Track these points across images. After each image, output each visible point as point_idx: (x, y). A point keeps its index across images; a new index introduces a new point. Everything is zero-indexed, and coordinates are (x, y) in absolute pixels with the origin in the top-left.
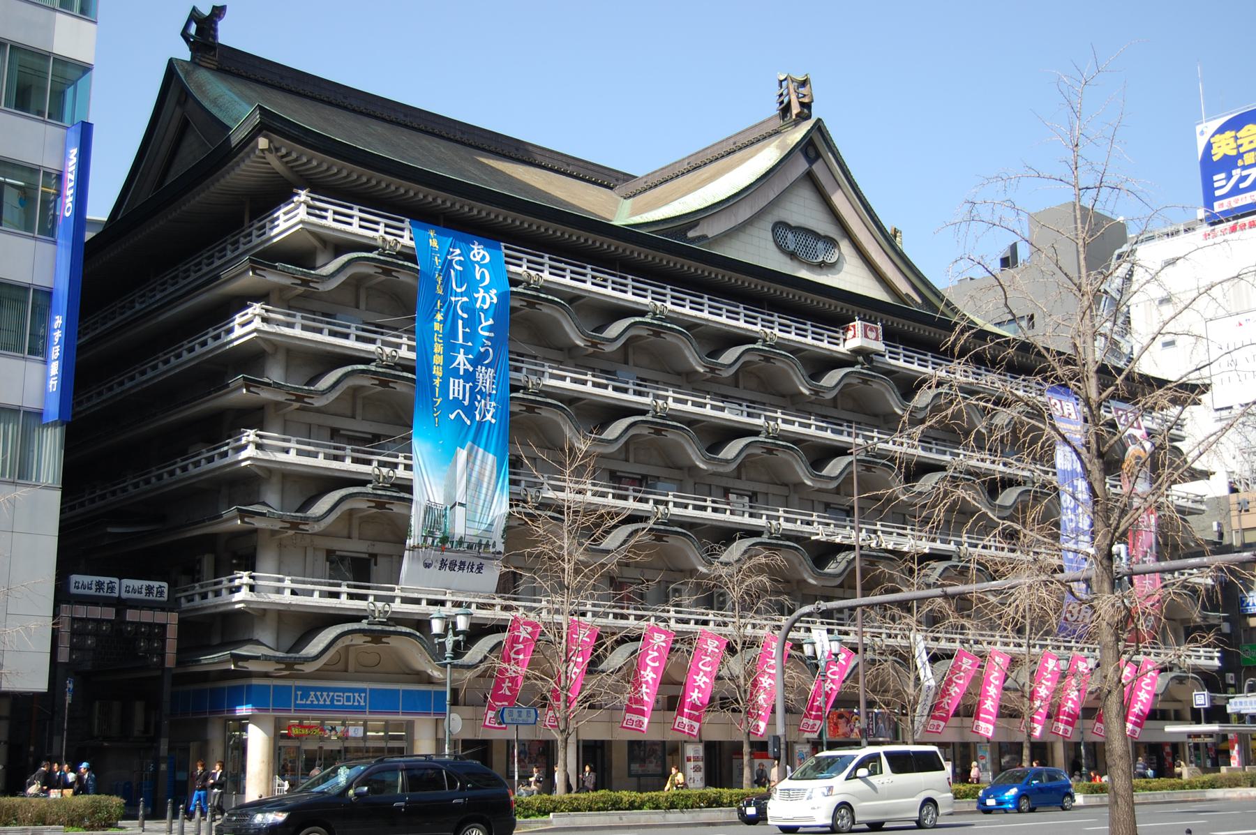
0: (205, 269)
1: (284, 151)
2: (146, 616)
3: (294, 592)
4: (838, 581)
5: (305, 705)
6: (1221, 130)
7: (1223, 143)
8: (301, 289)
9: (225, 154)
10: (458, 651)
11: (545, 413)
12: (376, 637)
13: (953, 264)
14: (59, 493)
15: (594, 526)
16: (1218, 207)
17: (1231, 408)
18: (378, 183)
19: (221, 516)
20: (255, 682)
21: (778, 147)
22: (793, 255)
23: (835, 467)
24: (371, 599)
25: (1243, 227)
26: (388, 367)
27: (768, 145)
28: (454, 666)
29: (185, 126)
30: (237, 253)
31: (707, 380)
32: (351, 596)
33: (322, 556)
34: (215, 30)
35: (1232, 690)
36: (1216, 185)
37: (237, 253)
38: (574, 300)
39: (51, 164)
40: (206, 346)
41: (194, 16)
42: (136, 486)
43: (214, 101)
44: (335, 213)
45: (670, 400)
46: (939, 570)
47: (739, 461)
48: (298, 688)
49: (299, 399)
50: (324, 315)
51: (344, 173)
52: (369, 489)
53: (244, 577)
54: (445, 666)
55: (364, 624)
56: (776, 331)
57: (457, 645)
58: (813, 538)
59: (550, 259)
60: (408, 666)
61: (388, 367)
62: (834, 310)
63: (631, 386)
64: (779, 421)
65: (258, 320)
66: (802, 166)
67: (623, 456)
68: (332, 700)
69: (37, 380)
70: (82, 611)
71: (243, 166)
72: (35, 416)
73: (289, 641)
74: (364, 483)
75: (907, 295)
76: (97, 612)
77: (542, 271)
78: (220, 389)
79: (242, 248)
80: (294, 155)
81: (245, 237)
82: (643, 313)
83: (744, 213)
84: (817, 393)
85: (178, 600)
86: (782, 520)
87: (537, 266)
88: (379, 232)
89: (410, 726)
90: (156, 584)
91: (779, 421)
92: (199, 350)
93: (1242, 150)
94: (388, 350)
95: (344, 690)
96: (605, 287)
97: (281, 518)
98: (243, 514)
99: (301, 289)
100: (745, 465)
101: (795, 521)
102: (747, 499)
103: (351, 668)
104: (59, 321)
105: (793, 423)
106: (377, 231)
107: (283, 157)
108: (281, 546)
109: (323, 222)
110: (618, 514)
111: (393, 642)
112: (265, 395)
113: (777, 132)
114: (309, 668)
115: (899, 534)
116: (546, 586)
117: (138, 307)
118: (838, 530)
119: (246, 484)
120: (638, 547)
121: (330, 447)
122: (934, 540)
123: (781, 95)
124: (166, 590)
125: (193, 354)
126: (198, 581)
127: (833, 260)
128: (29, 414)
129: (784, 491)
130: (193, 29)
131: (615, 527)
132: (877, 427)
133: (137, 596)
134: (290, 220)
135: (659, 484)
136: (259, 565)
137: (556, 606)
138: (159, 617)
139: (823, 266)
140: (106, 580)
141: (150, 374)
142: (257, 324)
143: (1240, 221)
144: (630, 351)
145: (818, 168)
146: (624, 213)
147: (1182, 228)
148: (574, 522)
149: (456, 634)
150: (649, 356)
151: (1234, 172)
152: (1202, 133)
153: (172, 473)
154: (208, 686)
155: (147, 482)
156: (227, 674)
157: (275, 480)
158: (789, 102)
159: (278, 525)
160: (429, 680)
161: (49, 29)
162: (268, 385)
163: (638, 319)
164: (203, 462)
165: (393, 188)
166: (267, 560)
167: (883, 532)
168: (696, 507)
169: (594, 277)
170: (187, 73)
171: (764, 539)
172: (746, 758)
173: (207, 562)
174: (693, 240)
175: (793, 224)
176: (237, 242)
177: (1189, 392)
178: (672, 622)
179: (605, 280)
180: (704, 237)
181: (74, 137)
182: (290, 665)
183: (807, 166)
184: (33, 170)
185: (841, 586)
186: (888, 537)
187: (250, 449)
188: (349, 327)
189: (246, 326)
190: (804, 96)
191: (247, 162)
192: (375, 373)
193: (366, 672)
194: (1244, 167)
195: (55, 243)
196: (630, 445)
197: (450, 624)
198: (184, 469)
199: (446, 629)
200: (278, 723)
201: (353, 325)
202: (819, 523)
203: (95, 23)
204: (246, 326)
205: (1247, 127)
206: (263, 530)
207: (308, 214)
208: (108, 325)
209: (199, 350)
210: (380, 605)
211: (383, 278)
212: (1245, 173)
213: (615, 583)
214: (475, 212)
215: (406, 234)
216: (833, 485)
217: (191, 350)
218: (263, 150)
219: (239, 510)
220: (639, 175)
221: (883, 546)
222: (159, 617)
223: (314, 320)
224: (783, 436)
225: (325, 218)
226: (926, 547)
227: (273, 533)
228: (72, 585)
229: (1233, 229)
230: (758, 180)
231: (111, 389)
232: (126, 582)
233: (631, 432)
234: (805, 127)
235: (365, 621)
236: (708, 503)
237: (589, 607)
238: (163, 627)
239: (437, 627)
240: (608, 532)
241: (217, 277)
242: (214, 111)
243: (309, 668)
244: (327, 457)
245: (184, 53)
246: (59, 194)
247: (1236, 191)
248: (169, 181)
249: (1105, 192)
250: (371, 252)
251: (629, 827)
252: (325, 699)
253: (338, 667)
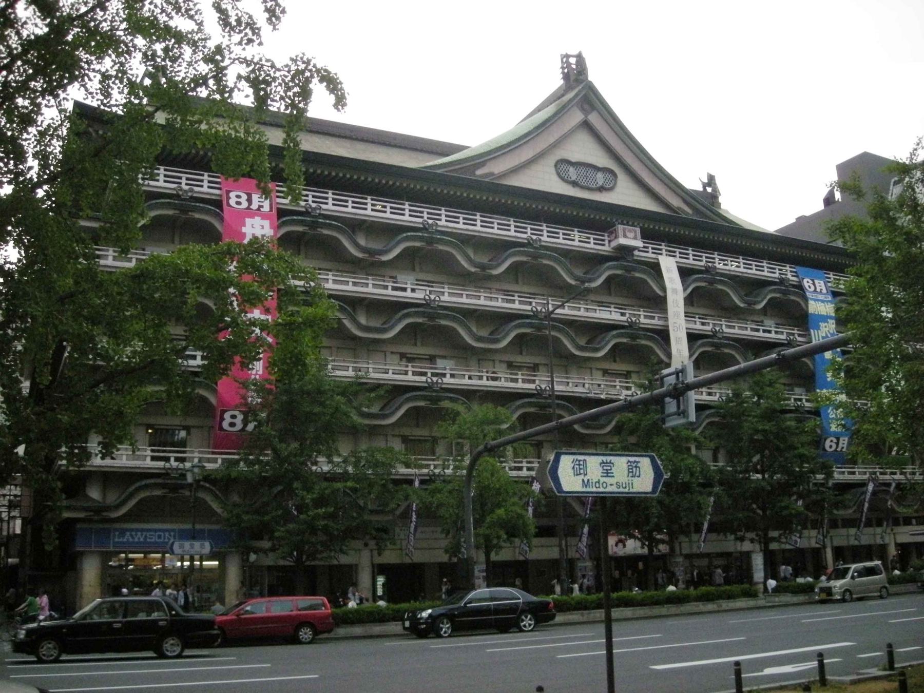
22: (574, 184)
38: (568, 255)
63: (773, 329)
75: (679, 208)
77: (542, 235)
95: (156, 531)
132: (643, 307)
172: (317, 563)
175: (573, 160)
179: (589, 238)
180: (492, 174)
183: (583, 116)
251: (726, 611)
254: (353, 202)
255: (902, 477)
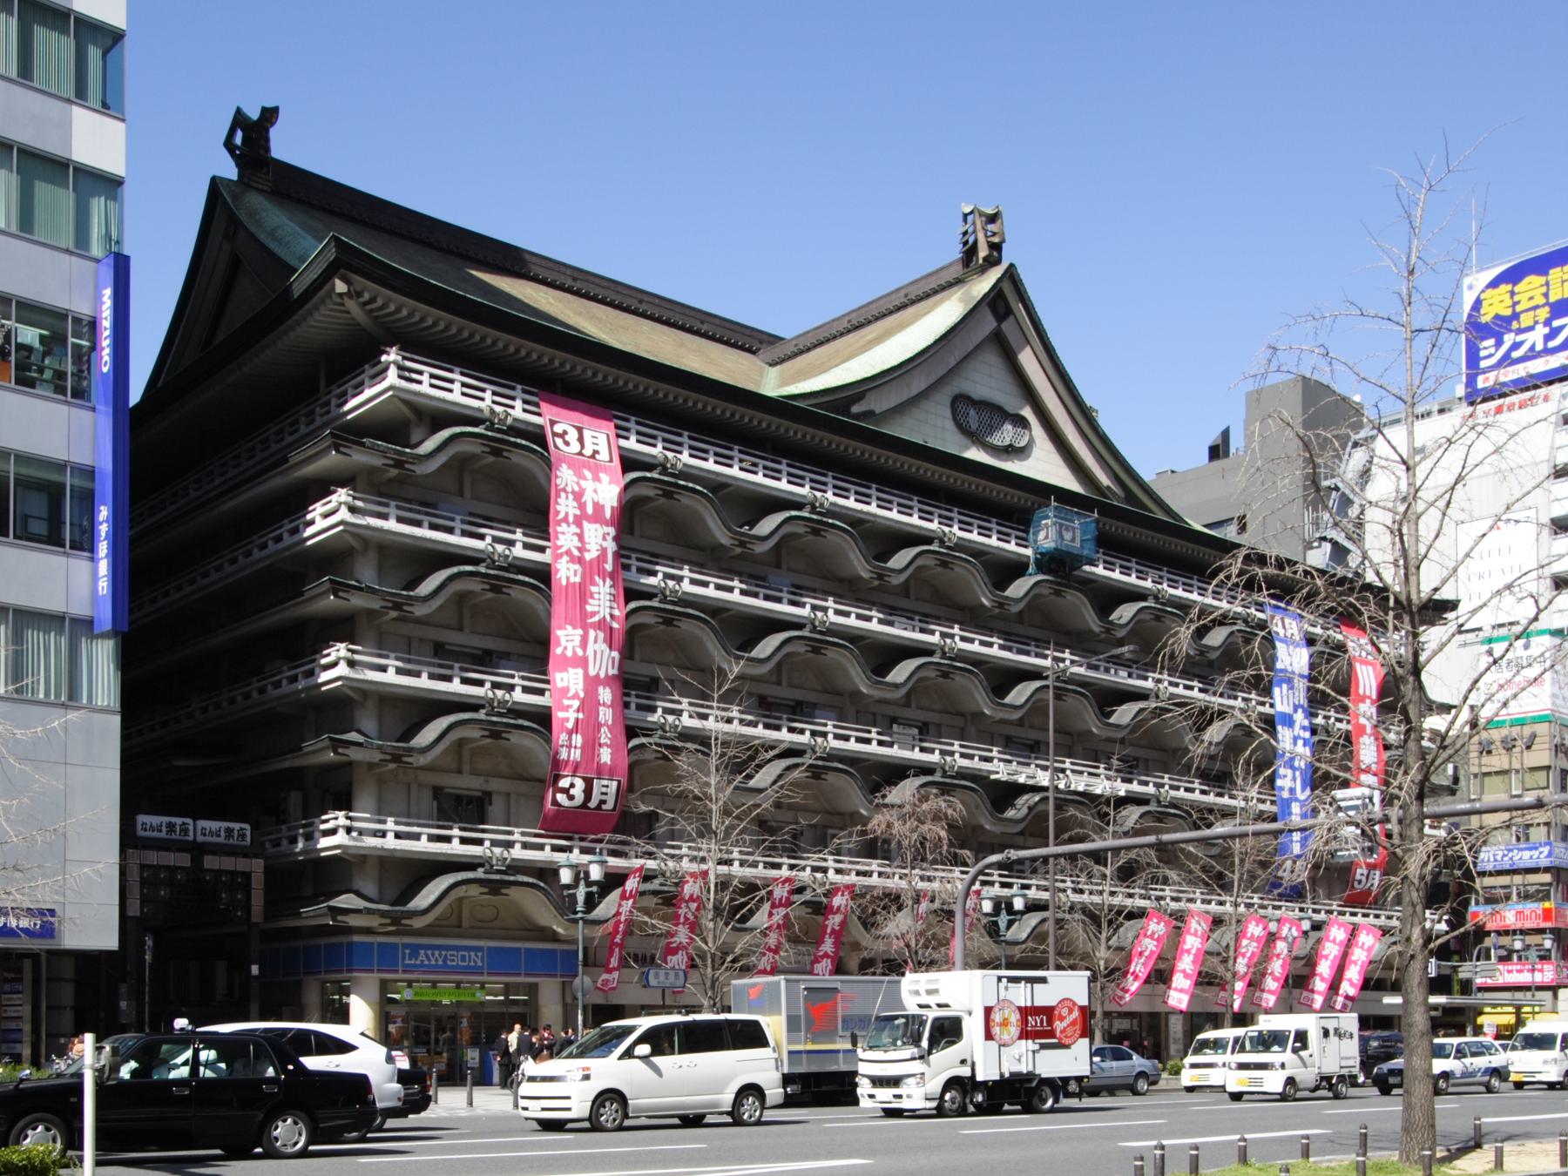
0: (274, 447)
1: (367, 296)
2: (227, 863)
3: (398, 836)
4: (1020, 827)
5: (415, 965)
6: (1494, 284)
7: (1495, 301)
8: (394, 472)
9: (285, 308)
10: (591, 903)
11: (686, 626)
12: (494, 887)
13: (1162, 449)
14: (118, 718)
15: (744, 759)
16: (1481, 383)
17: (1480, 629)
18: (483, 339)
19: (301, 749)
20: (356, 938)
21: (961, 300)
23: (1020, 694)
24: (487, 844)
25: (1511, 408)
26: (501, 568)
27: (936, 305)
28: (586, 922)
29: (235, 265)
30: (312, 427)
31: (873, 589)
32: (464, 841)
33: (427, 795)
34: (267, 140)
35: (1456, 957)
36: (1483, 353)
37: (312, 427)
39: (83, 308)
40: (267, 551)
41: (239, 120)
42: (204, 710)
43: (272, 234)
44: (432, 376)
45: (831, 612)
46: (1135, 817)
47: (910, 685)
48: (406, 946)
49: (397, 606)
50: (422, 504)
51: (442, 326)
52: (481, 715)
53: (338, 818)
54: (575, 921)
55: (480, 873)
56: (955, 529)
57: (589, 896)
58: (993, 777)
59: (690, 438)
60: (528, 919)
61: (501, 568)
62: (1016, 503)
64: (957, 639)
65: (344, 510)
66: (988, 323)
67: (774, 678)
68: (445, 960)
69: (83, 581)
70: (153, 857)
71: (317, 316)
72: (83, 626)
73: (393, 894)
74: (475, 708)
76: (171, 859)
78: (295, 597)
79: (319, 421)
80: (380, 302)
81: (322, 406)
82: (799, 506)
83: (918, 384)
84: (1001, 605)
85: (263, 844)
86: (957, 756)
87: (675, 447)
88: (486, 401)
89: (532, 990)
90: (236, 826)
91: (957, 639)
92: (272, 547)
93: (1518, 309)
94: (500, 548)
96: (755, 473)
97: (380, 748)
98: (337, 745)
99: (394, 472)
100: (916, 689)
101: (971, 757)
102: (916, 731)
103: (465, 923)
104: (104, 513)
105: (972, 641)
106: (482, 399)
107: (365, 304)
108: (381, 782)
109: (414, 387)
110: (773, 748)
111: (514, 893)
112: (357, 601)
113: (958, 282)
114: (418, 923)
115: (1090, 774)
116: (690, 829)
117: (193, 494)
118: (1020, 769)
119: (339, 707)
120: (795, 784)
121: (433, 665)
122: (1130, 781)
123: (965, 233)
124: (248, 833)
125: (265, 553)
126: (284, 822)
127: (1022, 444)
128: (76, 621)
129: (959, 722)
130: (238, 138)
131: (770, 761)
133: (214, 839)
134: (394, 380)
135: (817, 712)
136: (357, 802)
137: (701, 854)
138: (241, 864)
139: (1010, 451)
140: (178, 821)
141: (214, 577)
142: (344, 514)
143: (1508, 400)
144: (784, 551)
145: (1008, 327)
146: (773, 383)
147: (1435, 408)
148: (723, 755)
149: (589, 884)
150: (801, 562)
151: (1506, 337)
152: (1470, 287)
153: (247, 696)
154: (322, 941)
155: (218, 706)
156: (323, 930)
157: (371, 704)
158: (976, 242)
159: (377, 757)
160: (554, 937)
161: (66, 128)
162: (361, 589)
163: (794, 513)
164: (284, 682)
165: (500, 345)
166: (365, 797)
167: (1073, 771)
168: (859, 740)
169: (741, 461)
170: (235, 197)
171: (937, 777)
173: (295, 799)
174: (858, 416)
175: (975, 396)
176: (312, 412)
177: (1437, 609)
178: (831, 873)
181: (107, 273)
182: (396, 919)
184: (61, 315)
185: (1021, 833)
186: (1078, 777)
187: (337, 666)
188: (453, 520)
189: (327, 518)
190: (994, 234)
191: (323, 310)
192: (486, 576)
193: (478, 931)
194: (1520, 331)
195: (94, 409)
196: (783, 664)
197: (580, 874)
198: (262, 691)
199: (577, 879)
200: (384, 986)
201: (458, 517)
202: (1000, 760)
203: (123, 120)
204: (327, 518)
205: (1528, 279)
206: (359, 763)
207: (400, 377)
208: (158, 516)
209: (272, 547)
210: (497, 851)
211: (491, 459)
212: (1519, 338)
213: (763, 825)
214: (600, 377)
215: (518, 404)
216: (1016, 715)
217: (264, 546)
218: (341, 295)
219: (331, 739)
220: (788, 336)
221: (1073, 787)
222: (241, 864)
223: (410, 510)
224: (962, 656)
225: (420, 382)
226: (1122, 789)
227: (371, 766)
228: (139, 827)
229: (1499, 410)
230: (936, 342)
231: (166, 594)
232: (202, 823)
233: (787, 649)
234: (994, 275)
235: (481, 870)
236: (873, 735)
237: (735, 855)
238: (247, 875)
239: (566, 876)
240: (760, 766)
241: (286, 460)
242: (273, 246)
243: (418, 923)
244: (432, 677)
245: (230, 171)
246: (94, 347)
247: (1507, 361)
248: (221, 336)
249: (1444, 333)
250: (476, 425)
252: (436, 958)
253: (450, 923)
254: (432, 376)
255: (904, 884)
